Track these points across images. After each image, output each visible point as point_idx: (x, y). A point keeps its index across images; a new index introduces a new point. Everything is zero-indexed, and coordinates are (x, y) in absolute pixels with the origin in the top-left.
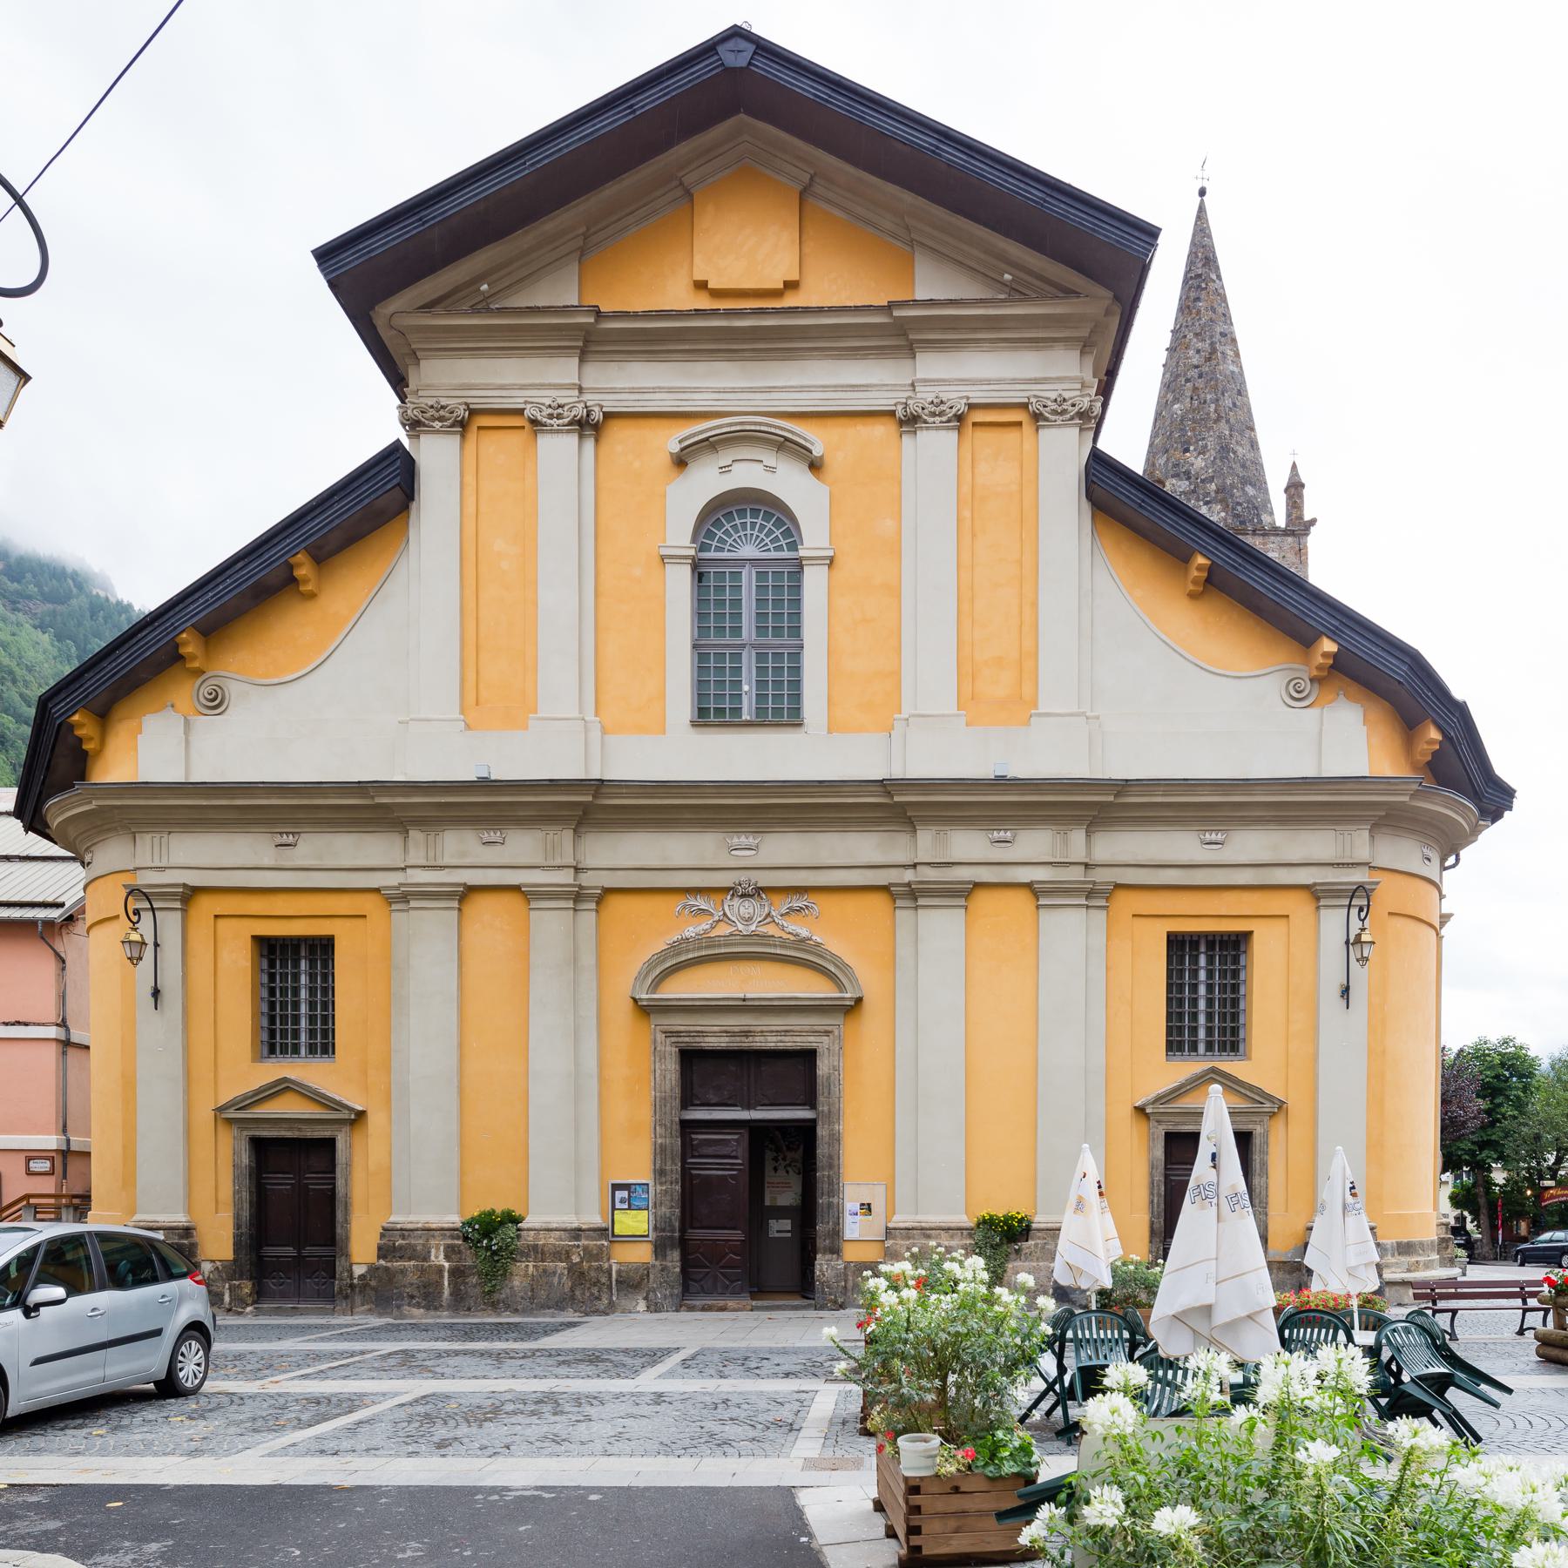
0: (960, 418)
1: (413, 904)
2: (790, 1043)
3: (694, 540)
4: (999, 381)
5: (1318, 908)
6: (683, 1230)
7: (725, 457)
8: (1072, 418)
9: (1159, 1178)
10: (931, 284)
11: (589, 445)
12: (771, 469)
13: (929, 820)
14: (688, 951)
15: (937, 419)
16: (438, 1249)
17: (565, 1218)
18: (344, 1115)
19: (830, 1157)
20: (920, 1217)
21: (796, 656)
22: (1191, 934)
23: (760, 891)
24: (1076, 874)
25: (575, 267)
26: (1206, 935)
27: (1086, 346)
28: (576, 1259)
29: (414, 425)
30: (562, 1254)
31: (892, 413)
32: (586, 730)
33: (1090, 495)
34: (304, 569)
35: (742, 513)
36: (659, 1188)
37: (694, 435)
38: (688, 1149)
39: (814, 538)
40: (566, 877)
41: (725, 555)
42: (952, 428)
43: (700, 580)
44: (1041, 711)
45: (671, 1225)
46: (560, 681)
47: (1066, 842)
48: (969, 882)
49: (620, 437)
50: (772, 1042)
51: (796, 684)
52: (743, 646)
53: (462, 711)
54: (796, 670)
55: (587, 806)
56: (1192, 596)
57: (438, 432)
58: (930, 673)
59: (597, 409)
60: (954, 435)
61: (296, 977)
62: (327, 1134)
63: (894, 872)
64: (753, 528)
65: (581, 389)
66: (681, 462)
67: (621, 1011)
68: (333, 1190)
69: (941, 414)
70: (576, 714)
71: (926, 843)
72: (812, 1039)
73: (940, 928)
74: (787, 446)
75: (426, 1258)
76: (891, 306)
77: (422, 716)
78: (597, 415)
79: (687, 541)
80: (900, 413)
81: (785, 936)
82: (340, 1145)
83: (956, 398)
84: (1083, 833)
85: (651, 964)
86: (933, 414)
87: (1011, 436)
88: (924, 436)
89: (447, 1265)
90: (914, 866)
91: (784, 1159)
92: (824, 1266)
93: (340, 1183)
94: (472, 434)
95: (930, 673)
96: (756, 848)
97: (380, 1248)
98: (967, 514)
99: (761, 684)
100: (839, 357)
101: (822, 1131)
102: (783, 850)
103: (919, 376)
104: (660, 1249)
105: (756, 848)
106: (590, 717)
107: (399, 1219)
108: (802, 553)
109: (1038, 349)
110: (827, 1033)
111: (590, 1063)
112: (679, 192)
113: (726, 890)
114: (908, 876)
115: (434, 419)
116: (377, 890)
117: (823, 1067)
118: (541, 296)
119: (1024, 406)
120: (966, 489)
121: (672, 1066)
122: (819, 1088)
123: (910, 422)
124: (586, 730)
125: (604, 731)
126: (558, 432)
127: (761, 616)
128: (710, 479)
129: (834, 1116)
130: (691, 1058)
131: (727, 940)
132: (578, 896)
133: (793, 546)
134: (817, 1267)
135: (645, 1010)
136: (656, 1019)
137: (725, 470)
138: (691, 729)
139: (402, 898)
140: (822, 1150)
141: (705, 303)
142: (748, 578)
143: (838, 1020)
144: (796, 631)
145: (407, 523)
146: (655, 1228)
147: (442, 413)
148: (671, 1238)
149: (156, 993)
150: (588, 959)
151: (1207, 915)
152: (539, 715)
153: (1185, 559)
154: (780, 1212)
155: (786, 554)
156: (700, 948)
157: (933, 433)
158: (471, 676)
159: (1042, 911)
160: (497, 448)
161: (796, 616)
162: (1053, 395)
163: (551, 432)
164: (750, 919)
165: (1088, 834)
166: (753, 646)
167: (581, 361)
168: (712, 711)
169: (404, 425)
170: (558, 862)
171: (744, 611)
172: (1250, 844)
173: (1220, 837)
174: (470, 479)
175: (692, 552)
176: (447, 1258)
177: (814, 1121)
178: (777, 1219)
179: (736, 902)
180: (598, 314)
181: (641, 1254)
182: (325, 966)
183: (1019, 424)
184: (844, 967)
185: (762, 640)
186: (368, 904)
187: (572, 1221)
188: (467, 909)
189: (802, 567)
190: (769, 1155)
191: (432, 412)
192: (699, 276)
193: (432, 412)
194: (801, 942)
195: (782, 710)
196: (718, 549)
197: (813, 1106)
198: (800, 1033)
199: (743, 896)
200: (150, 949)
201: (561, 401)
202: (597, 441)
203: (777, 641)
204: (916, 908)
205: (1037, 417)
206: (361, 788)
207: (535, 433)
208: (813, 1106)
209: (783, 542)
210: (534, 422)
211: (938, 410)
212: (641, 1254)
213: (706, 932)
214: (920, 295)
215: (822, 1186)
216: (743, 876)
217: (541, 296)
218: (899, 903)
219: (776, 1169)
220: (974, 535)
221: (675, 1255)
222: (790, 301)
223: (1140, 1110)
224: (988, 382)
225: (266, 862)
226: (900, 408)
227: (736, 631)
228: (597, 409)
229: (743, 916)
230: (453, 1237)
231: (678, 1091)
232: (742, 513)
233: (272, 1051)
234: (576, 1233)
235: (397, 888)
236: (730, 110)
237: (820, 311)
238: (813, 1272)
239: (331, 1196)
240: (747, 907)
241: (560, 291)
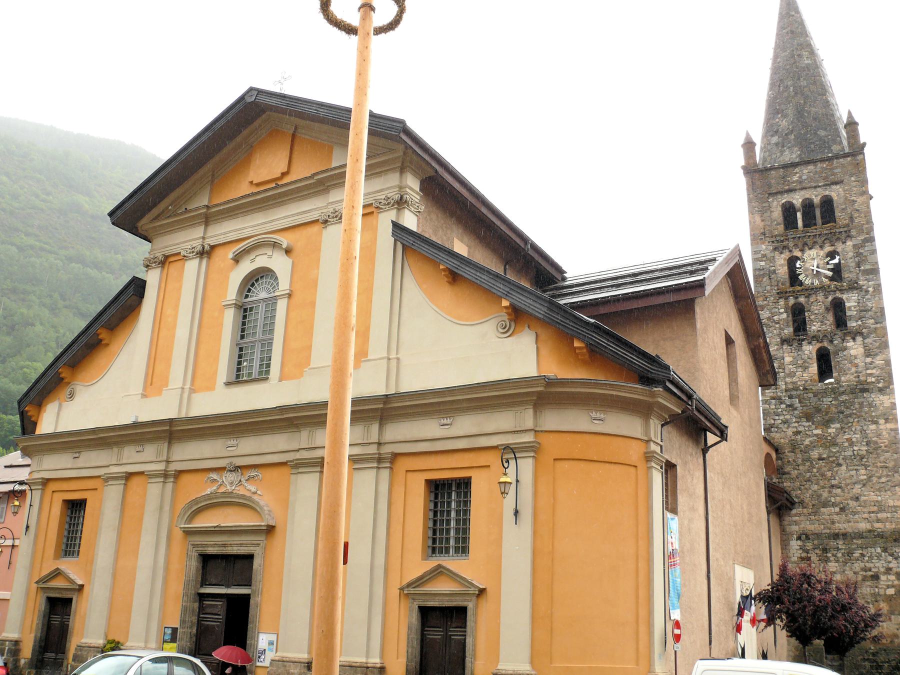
1: (110, 483)
2: (243, 551)
5: (705, 451)
7: (252, 256)
9: (416, 637)
13: (305, 425)
18: (472, 590)
22: (448, 479)
23: (237, 468)
26: (453, 480)
38: (201, 609)
40: (373, 449)
44: (369, 358)
49: (219, 253)
52: (255, 341)
55: (171, 432)
61: (449, 503)
63: (292, 454)
67: (178, 534)
70: (385, 355)
74: (275, 245)
78: (207, 248)
84: (166, 445)
85: (185, 509)
90: (298, 450)
102: (249, 447)
117: (257, 562)
130: (206, 559)
135: (188, 533)
137: (253, 261)
143: (262, 537)
149: (516, 513)
151: (446, 469)
162: (383, 197)
168: (239, 377)
172: (466, 425)
173: (449, 421)
177: (249, 595)
188: (129, 484)
198: (246, 545)
200: (513, 486)
204: (378, 468)
225: (69, 466)
233: (434, 550)
239: (463, 645)
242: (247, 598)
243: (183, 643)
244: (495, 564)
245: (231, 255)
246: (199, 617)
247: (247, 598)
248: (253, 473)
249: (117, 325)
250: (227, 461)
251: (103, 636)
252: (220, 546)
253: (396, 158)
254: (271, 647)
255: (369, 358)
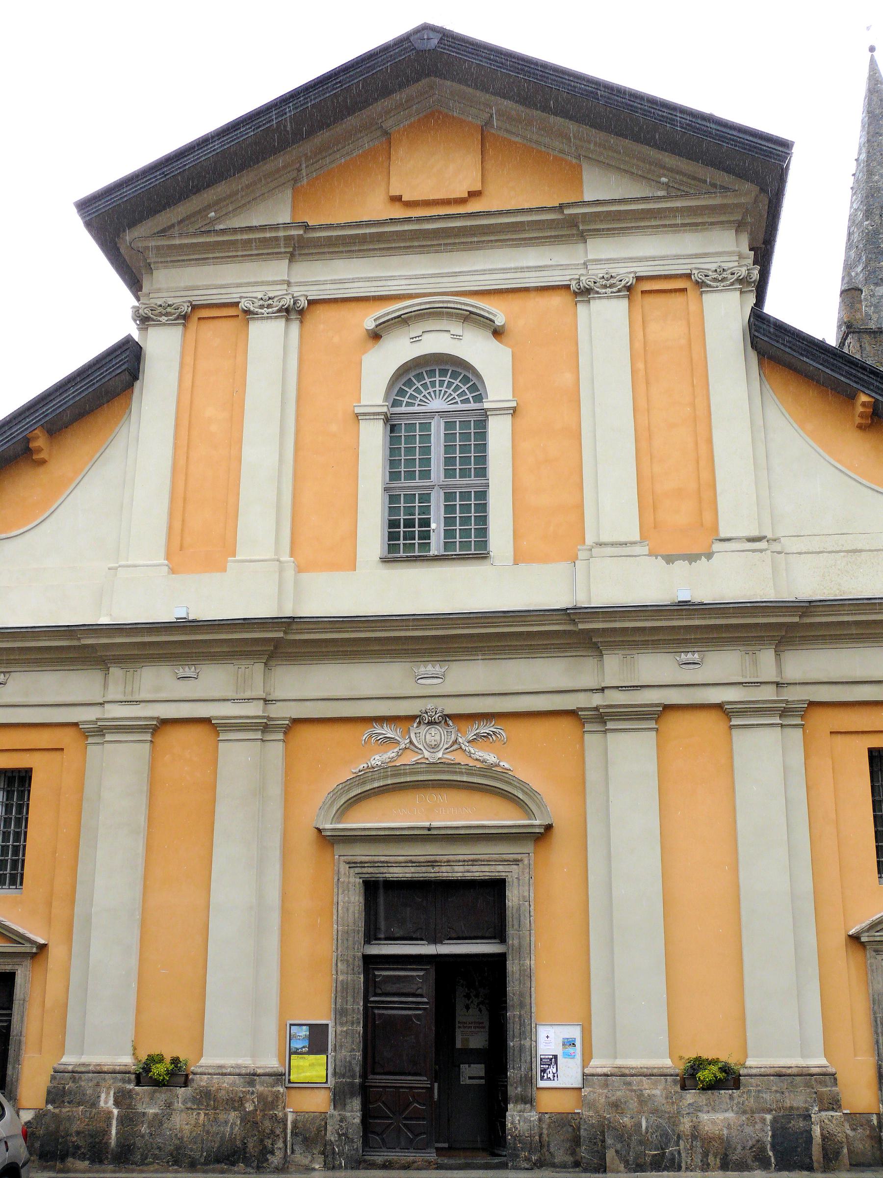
0: (629, 288)
1: (108, 737)
2: (478, 872)
3: (386, 398)
4: (662, 258)
6: (364, 1076)
7: (416, 330)
8: (732, 284)
10: (599, 187)
11: (295, 327)
12: (457, 337)
13: (614, 645)
14: (373, 780)
15: (609, 290)
16: (108, 1094)
17: (240, 1061)
19: (521, 995)
20: (620, 1062)
21: (482, 495)
23: (448, 718)
24: (767, 694)
25: (289, 193)
27: (739, 227)
28: (249, 1107)
29: (144, 320)
30: (235, 1102)
31: (568, 287)
32: (281, 571)
33: (754, 346)
34: (40, 442)
35: (431, 373)
36: (339, 1029)
37: (388, 314)
38: (371, 986)
39: (498, 390)
40: (254, 710)
41: (416, 409)
42: (623, 297)
43: (392, 431)
45: (351, 1070)
46: (260, 525)
47: (755, 663)
48: (657, 705)
50: (459, 872)
51: (483, 520)
52: (433, 487)
53: (168, 556)
54: (483, 508)
55: (278, 641)
56: (860, 427)
57: (164, 324)
58: (612, 503)
59: (302, 299)
60: (625, 303)
62: (8, 968)
63: (581, 695)
64: (441, 385)
65: (289, 284)
66: (376, 336)
67: (305, 839)
68: (8, 1028)
69: (611, 286)
70: (270, 555)
71: (614, 668)
72: (500, 868)
73: (630, 756)
74: (470, 318)
75: (94, 1104)
76: (561, 207)
77: (130, 563)
79: (380, 401)
80: (574, 286)
81: (472, 763)
82: (19, 980)
83: (626, 273)
84: (773, 651)
85: (335, 794)
86: (605, 287)
87: (677, 301)
88: (597, 305)
89: (116, 1111)
90: (603, 689)
91: (477, 996)
92: (518, 1119)
93: (15, 1019)
94: (193, 323)
95: (612, 503)
96: (442, 677)
97: (49, 1092)
98: (641, 365)
99: (449, 521)
100: (517, 246)
101: (512, 967)
102: (471, 679)
103: (590, 257)
104: (339, 1097)
105: (442, 677)
106: (286, 558)
107: (70, 1059)
108: (486, 405)
109: (696, 231)
110: (516, 862)
111: (273, 896)
112: (379, 133)
113: (413, 718)
114: (597, 700)
115: (161, 314)
116: (76, 725)
117: (513, 897)
118: (257, 218)
119: (688, 276)
120: (638, 345)
121: (355, 899)
122: (509, 919)
123: (584, 293)
124: (281, 571)
125: (299, 569)
126: (268, 318)
127: (449, 461)
128: (400, 349)
129: (524, 951)
130: (373, 889)
131: (414, 768)
132: (266, 727)
133: (479, 399)
134: (509, 1118)
135: (329, 840)
136: (340, 850)
137: (416, 340)
138: (381, 565)
139: (100, 730)
140: (512, 988)
141: (398, 212)
142: (437, 430)
144: (482, 472)
145: (131, 399)
146: (335, 1074)
147: (169, 310)
148: (352, 1084)
150: (275, 790)
152: (237, 558)
153: (851, 397)
154: (472, 1056)
155: (472, 405)
156: (386, 777)
157: (605, 301)
158: (177, 525)
159: (734, 732)
160: (214, 335)
161: (482, 459)
162: (713, 267)
163: (263, 318)
164: (436, 746)
165: (778, 654)
166: (441, 487)
167: (290, 261)
168: (405, 538)
169: (135, 321)
170: (248, 694)
171: (433, 456)
174: (189, 360)
175: (385, 409)
176: (117, 1103)
178: (469, 1063)
179: (423, 729)
180: (306, 227)
181: (318, 1102)
182: (21, 796)
183: (684, 290)
184: (532, 793)
185: (450, 481)
186: (65, 738)
187: (247, 1062)
189: (487, 416)
190: (460, 992)
191: (160, 309)
192: (394, 192)
193: (160, 309)
194: (488, 770)
195: (469, 542)
196: (408, 404)
197: (503, 939)
198: (488, 862)
199: (430, 723)
201: (271, 295)
202: (301, 322)
203: (465, 481)
204: (605, 732)
205: (700, 284)
206: (70, 631)
207: (248, 321)
208: (503, 939)
209: (469, 396)
210: (247, 312)
211: (608, 283)
212: (318, 1102)
213: (392, 760)
214: (587, 197)
215: (513, 1028)
216: (430, 705)
217: (257, 218)
218: (588, 727)
219: (467, 1007)
220: (648, 383)
221: (356, 1104)
222: (474, 207)
223: (855, 939)
224: (653, 259)
226: (573, 283)
227: (426, 475)
228: (302, 299)
229: (431, 745)
230: (124, 1081)
231: (361, 924)
232: (431, 373)
234: (251, 1077)
235: (95, 722)
236: (418, 81)
237: (500, 213)
238: (504, 1125)
240: (434, 734)
241: (277, 212)
242: (500, 961)
243: (344, 1053)
244: (67, 899)
245: (370, 324)
246: (366, 1000)
247: (500, 961)
248: (485, 728)
249: (67, 425)
250: (430, 705)
251: (130, 1049)
252: (419, 864)
253: (737, 206)
254: (571, 1050)
255: (237, 558)
